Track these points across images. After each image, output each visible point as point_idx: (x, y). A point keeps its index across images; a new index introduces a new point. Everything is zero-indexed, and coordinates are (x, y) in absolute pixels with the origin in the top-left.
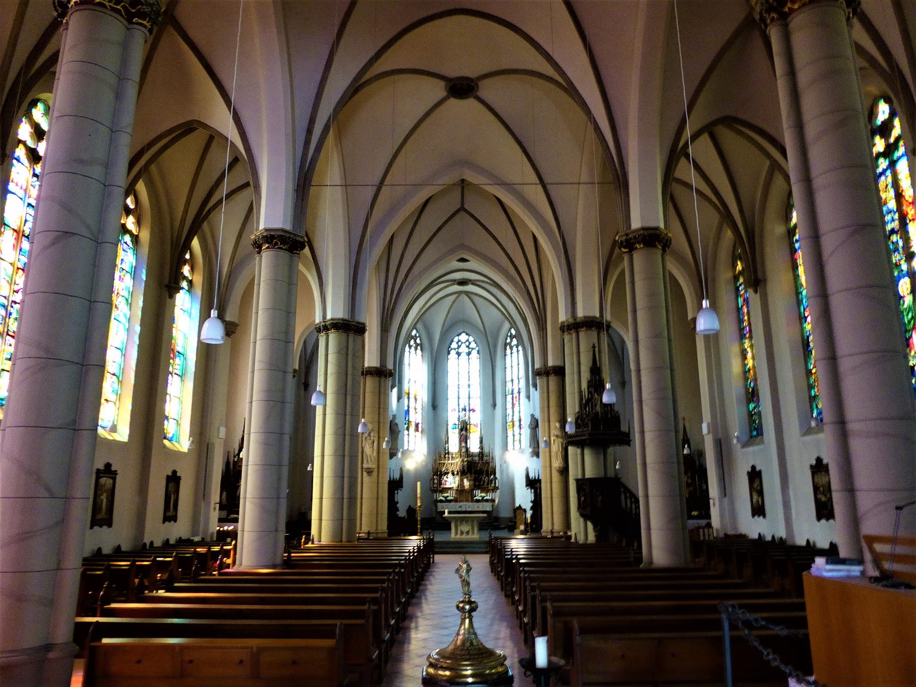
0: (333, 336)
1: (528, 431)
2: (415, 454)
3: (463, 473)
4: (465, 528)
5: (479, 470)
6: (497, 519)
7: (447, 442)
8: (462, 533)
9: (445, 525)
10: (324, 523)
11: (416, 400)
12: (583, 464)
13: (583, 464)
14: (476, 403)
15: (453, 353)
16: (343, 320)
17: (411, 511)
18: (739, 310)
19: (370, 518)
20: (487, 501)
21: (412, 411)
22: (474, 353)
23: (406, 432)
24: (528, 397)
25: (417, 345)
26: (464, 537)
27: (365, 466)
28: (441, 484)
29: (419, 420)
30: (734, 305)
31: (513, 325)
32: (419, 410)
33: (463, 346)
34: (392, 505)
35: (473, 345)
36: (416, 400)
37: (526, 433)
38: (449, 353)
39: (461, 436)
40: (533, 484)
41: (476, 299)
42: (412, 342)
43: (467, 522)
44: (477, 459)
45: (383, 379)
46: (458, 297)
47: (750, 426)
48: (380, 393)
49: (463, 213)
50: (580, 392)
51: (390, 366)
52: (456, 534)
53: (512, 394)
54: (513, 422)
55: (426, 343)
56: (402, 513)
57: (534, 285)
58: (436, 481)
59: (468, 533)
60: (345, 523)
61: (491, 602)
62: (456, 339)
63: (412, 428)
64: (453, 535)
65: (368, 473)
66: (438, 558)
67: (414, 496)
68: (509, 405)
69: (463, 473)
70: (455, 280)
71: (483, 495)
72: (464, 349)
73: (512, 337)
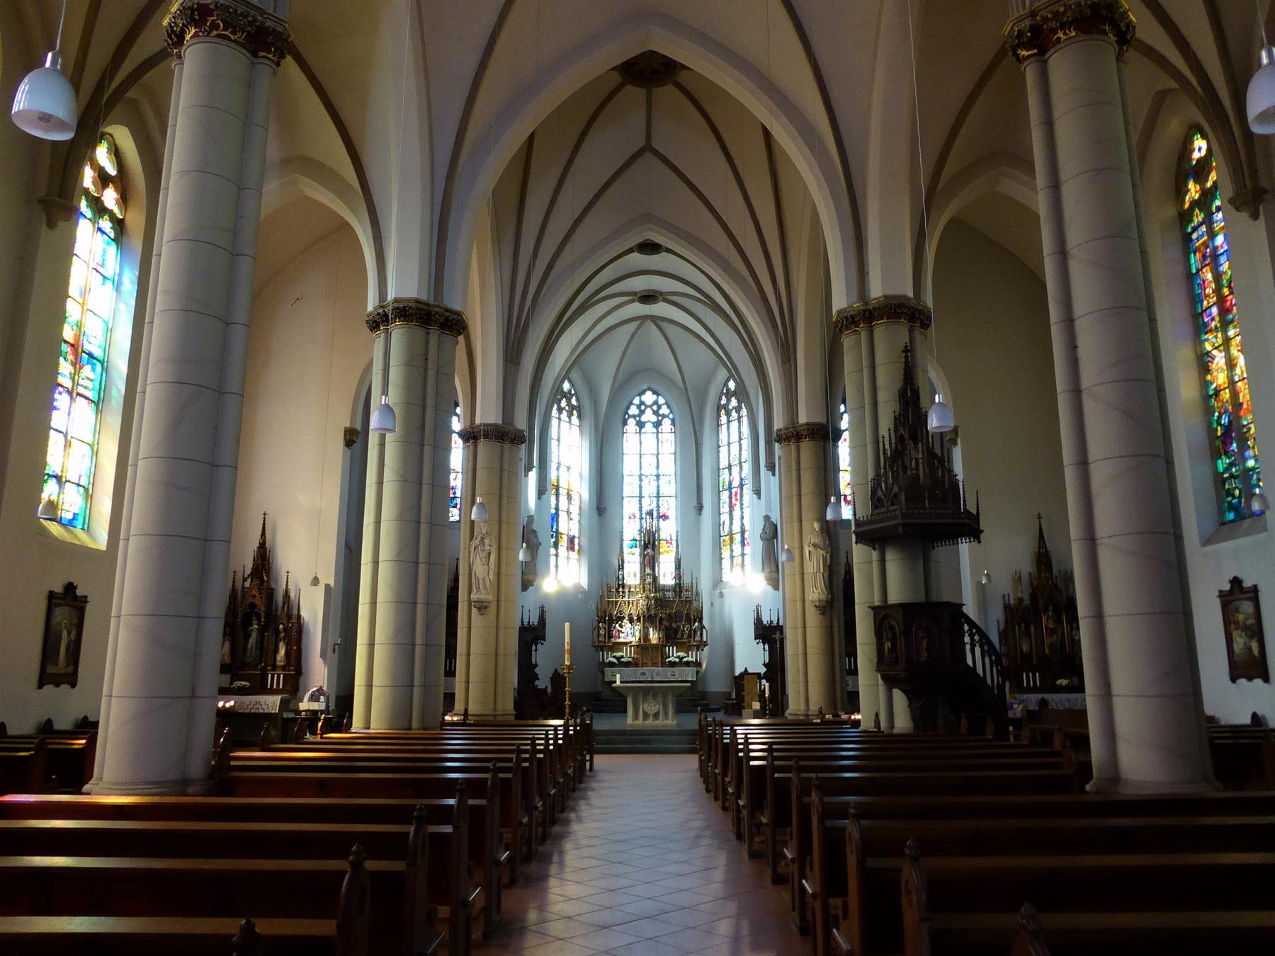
0: (398, 333)
1: (759, 544)
2: (565, 575)
3: (648, 619)
4: (651, 707)
5: (676, 614)
6: (704, 695)
7: (621, 567)
8: (646, 715)
9: (614, 702)
10: (376, 692)
11: (569, 497)
12: (881, 579)
13: (881, 579)
14: (670, 506)
15: (632, 422)
16: (417, 301)
17: (557, 679)
18: (1191, 278)
19: (480, 682)
20: (688, 664)
21: (563, 517)
22: (667, 424)
23: (553, 551)
24: (757, 492)
25: (572, 408)
26: (650, 722)
27: (474, 597)
28: (610, 636)
29: (575, 531)
30: (1179, 270)
31: (734, 373)
32: (575, 516)
33: (649, 411)
34: (527, 669)
35: (664, 410)
36: (569, 497)
37: (755, 548)
38: (625, 423)
39: (643, 556)
40: (768, 633)
41: (671, 330)
42: (564, 403)
43: (654, 697)
44: (670, 595)
45: (507, 446)
46: (640, 326)
47: (1220, 501)
48: (501, 470)
49: (649, 156)
50: (876, 442)
51: (521, 423)
52: (636, 717)
53: (730, 488)
54: (731, 534)
55: (587, 405)
56: (543, 682)
57: (774, 282)
58: (602, 632)
59: (656, 716)
60: (417, 691)
61: (719, 875)
62: (636, 401)
63: (564, 542)
64: (630, 720)
65: (479, 609)
66: (599, 760)
67: (560, 650)
68: (725, 508)
69: (648, 619)
70: (634, 294)
72: (649, 416)
73: (729, 395)
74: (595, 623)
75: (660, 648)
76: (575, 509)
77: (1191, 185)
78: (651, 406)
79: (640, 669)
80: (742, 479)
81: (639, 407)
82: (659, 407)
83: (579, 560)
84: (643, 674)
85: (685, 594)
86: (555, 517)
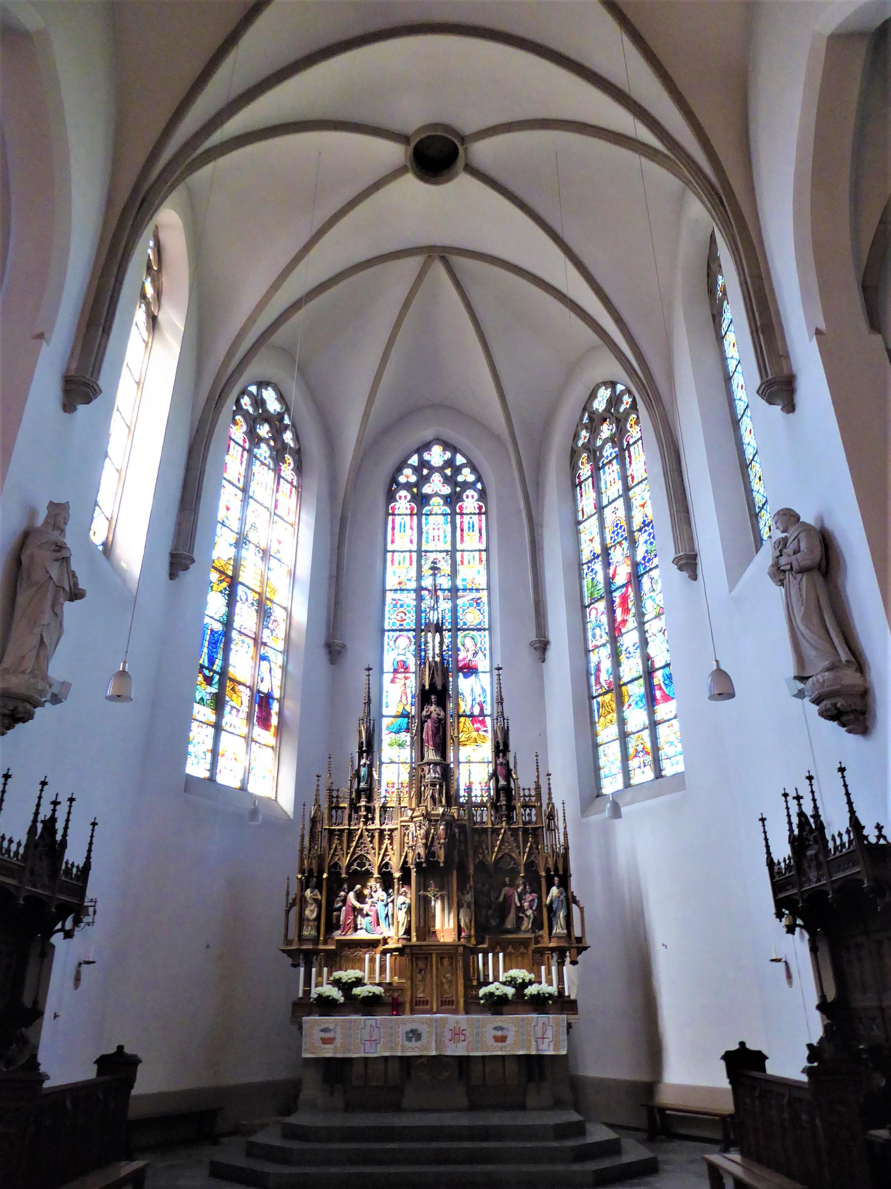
3: (428, 873)
5: (503, 867)
11: (263, 610)
20: (540, 1003)
22: (470, 502)
33: (437, 477)
38: (391, 497)
44: (485, 817)
54: (617, 688)
58: (311, 912)
62: (414, 460)
63: (239, 702)
68: (599, 635)
71: (521, 974)
72: (436, 485)
74: (295, 889)
75: (461, 955)
76: (275, 640)
78: (441, 470)
79: (408, 1020)
80: (635, 565)
81: (417, 470)
82: (457, 470)
83: (277, 750)
84: (414, 1035)
85: (521, 816)
86: (223, 640)
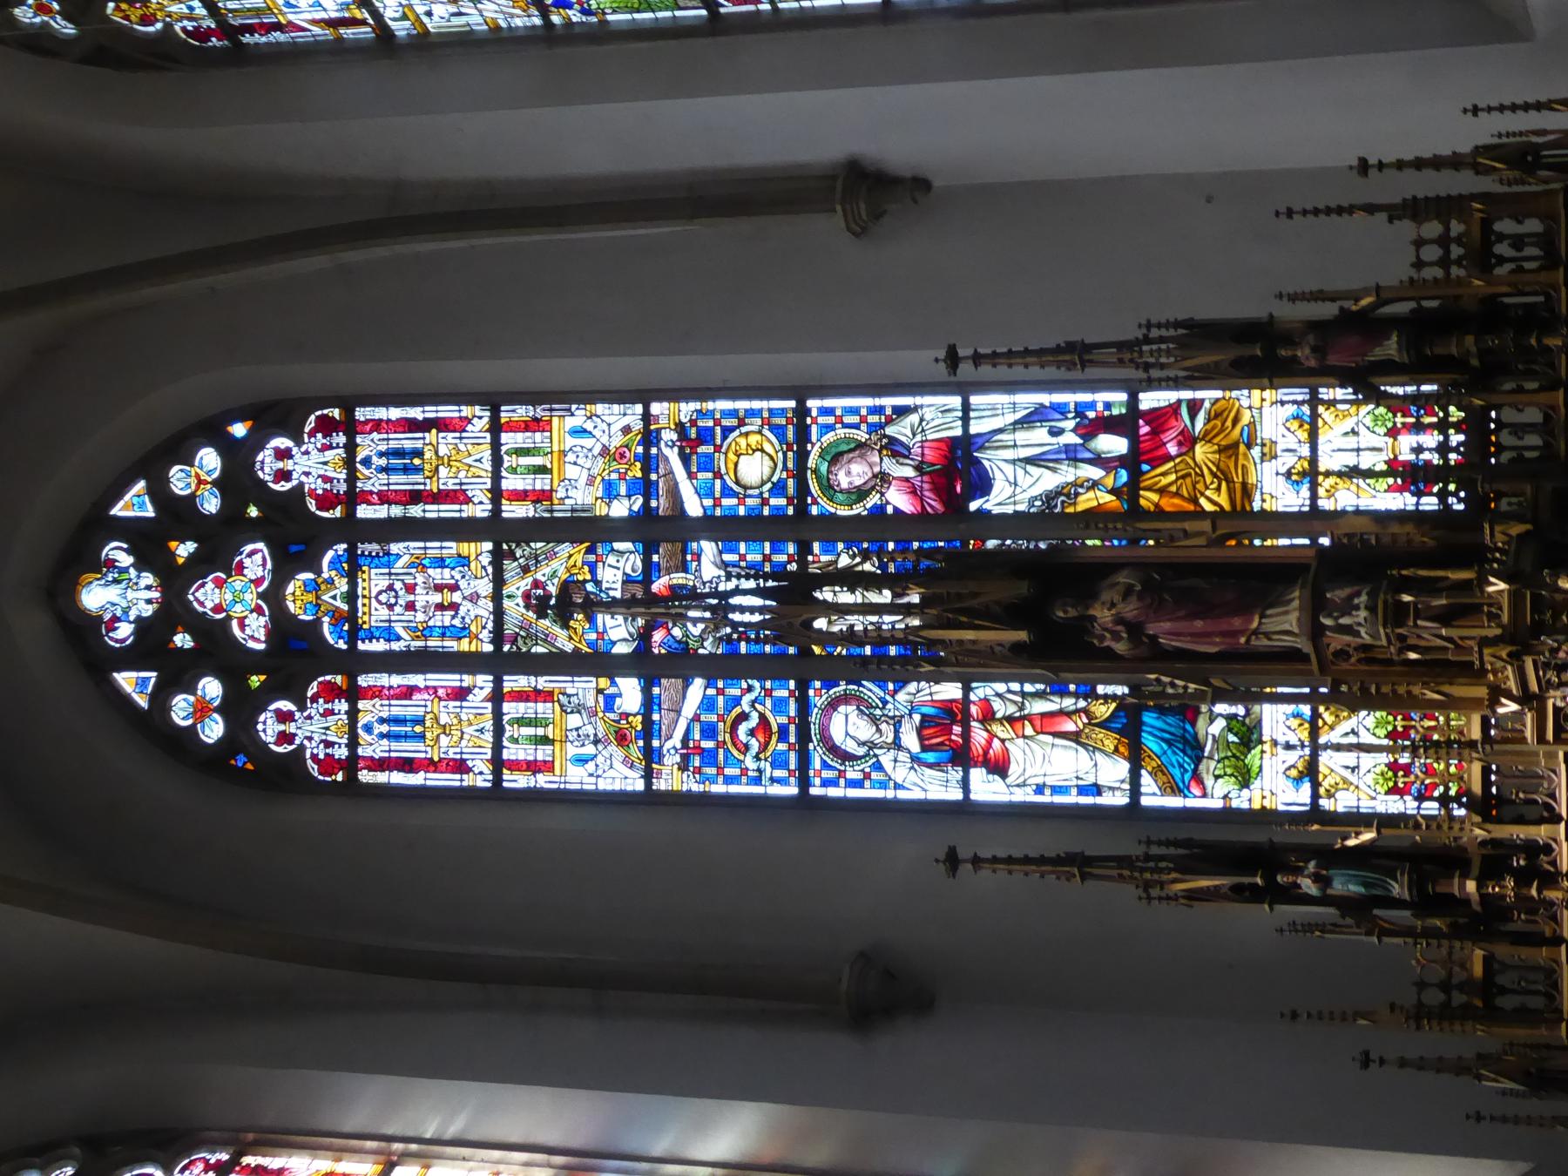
14: (875, 445)
15: (310, 728)
22: (311, 464)
33: (206, 596)
38: (285, 774)
72: (237, 598)
77: (1461, 437)
81: (178, 674)
82: (177, 514)
